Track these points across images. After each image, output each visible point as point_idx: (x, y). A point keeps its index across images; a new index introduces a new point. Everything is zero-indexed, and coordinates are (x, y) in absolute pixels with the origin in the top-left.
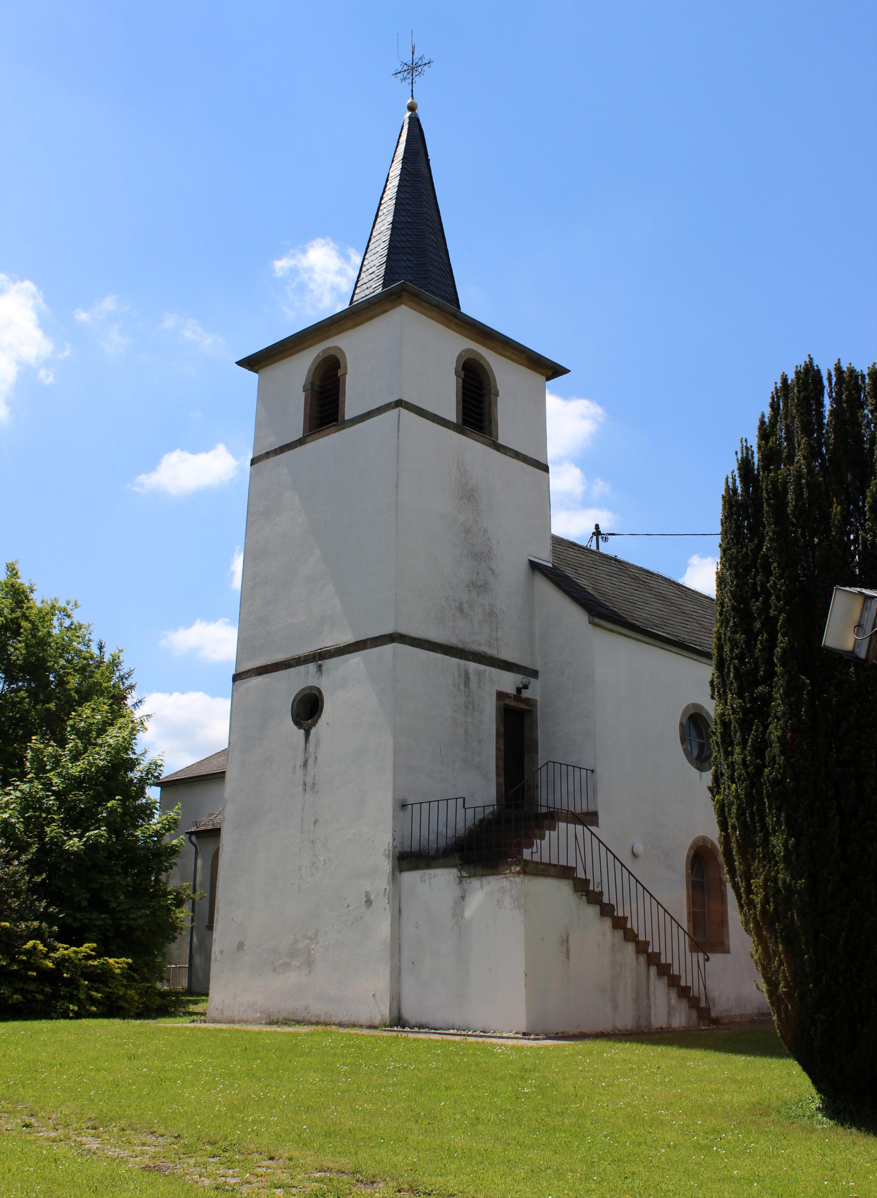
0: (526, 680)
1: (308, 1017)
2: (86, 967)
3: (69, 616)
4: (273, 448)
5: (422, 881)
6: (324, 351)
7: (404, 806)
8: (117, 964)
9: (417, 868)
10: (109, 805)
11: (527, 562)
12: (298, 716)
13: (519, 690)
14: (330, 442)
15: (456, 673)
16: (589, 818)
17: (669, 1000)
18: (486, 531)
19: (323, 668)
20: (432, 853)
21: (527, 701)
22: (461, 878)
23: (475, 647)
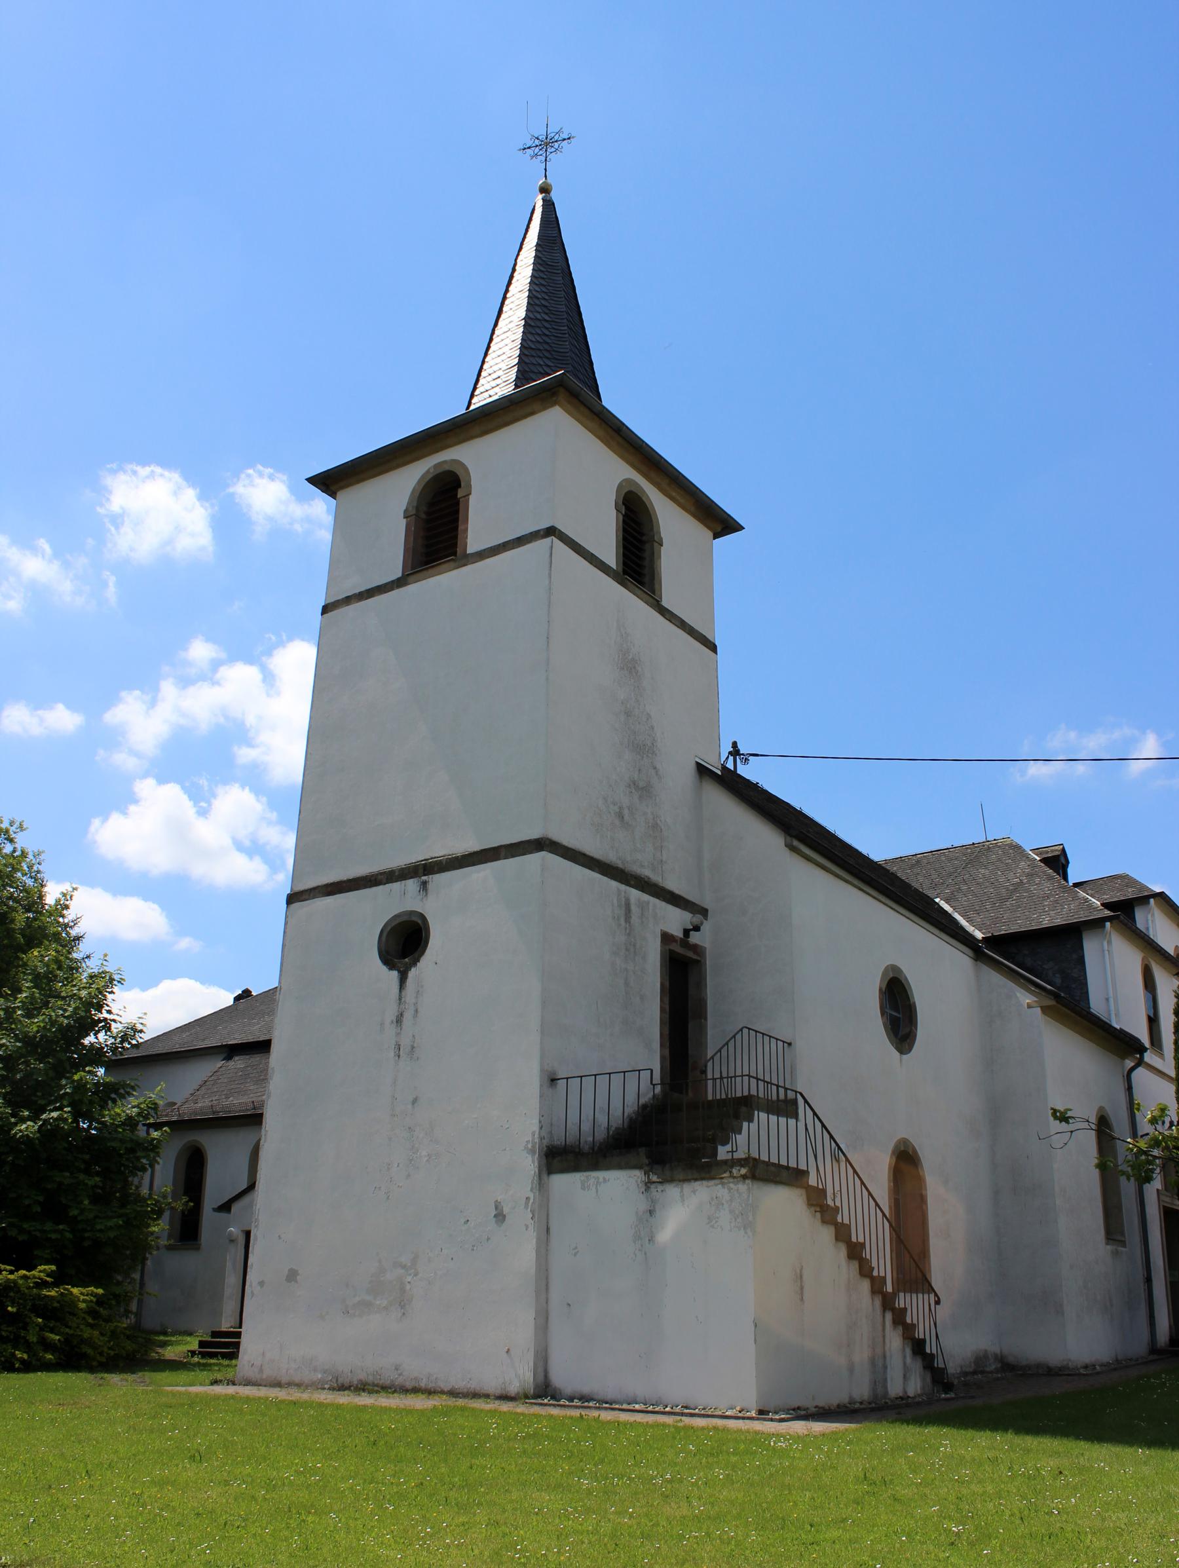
0: (698, 918)
1: (399, 1381)
2: (40, 1297)
3: (11, 841)
4: (357, 591)
5: (583, 1188)
6: (435, 466)
7: (553, 1080)
8: (81, 1294)
9: (576, 1169)
10: (76, 1077)
11: (693, 766)
12: (388, 952)
13: (686, 932)
14: (445, 583)
15: (615, 901)
16: (786, 1107)
17: (905, 1357)
18: (649, 716)
19: (430, 886)
20: (586, 1148)
21: (695, 948)
22: (648, 1184)
23: (636, 869)
